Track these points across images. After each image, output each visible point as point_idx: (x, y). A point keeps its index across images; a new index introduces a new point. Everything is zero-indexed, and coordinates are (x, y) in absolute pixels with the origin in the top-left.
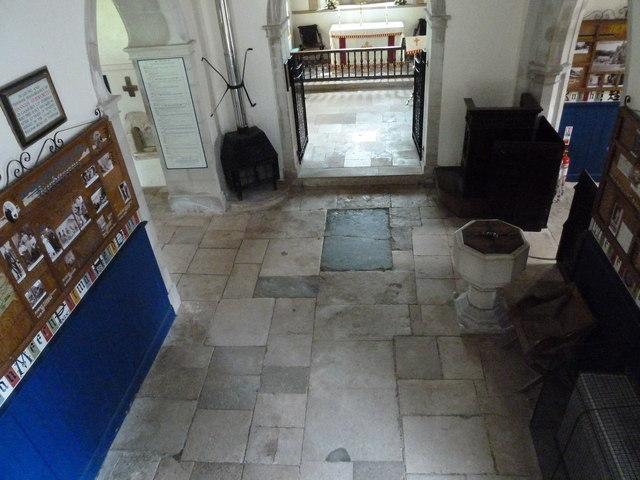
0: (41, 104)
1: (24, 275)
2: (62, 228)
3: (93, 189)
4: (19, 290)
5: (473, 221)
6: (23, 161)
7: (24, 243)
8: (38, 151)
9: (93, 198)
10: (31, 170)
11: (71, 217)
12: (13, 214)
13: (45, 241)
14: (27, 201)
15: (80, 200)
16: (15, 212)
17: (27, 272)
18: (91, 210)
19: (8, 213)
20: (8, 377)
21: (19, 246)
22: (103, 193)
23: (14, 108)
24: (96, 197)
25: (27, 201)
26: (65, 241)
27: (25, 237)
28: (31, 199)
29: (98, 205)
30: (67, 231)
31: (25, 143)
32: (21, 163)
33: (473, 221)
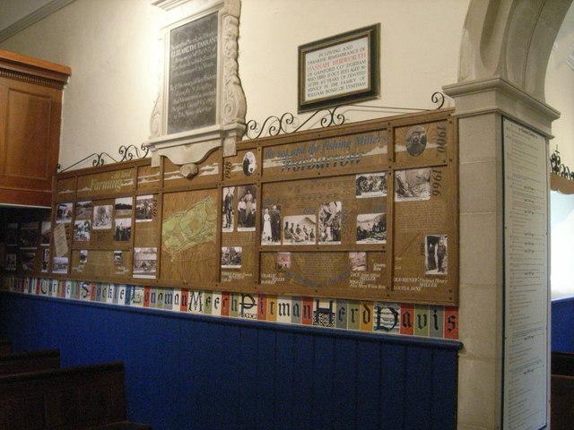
0: (345, 68)
1: (232, 230)
2: (293, 220)
3: (369, 206)
4: (221, 238)
5: (368, 154)
6: (284, 120)
7: (246, 201)
8: (314, 121)
9: (361, 217)
10: (287, 136)
11: (313, 218)
12: (250, 166)
13: (267, 217)
14: (268, 164)
15: (337, 207)
16: (253, 166)
17: (235, 229)
18: (345, 231)
19: (247, 163)
20: (445, 276)
21: (240, 200)
22: (382, 225)
23: (307, 66)
24: (367, 220)
25: (268, 164)
26: (288, 237)
27: (250, 197)
28: (275, 165)
29: (363, 235)
30: (298, 231)
31: (304, 107)
32: (281, 121)
33: (368, 154)
